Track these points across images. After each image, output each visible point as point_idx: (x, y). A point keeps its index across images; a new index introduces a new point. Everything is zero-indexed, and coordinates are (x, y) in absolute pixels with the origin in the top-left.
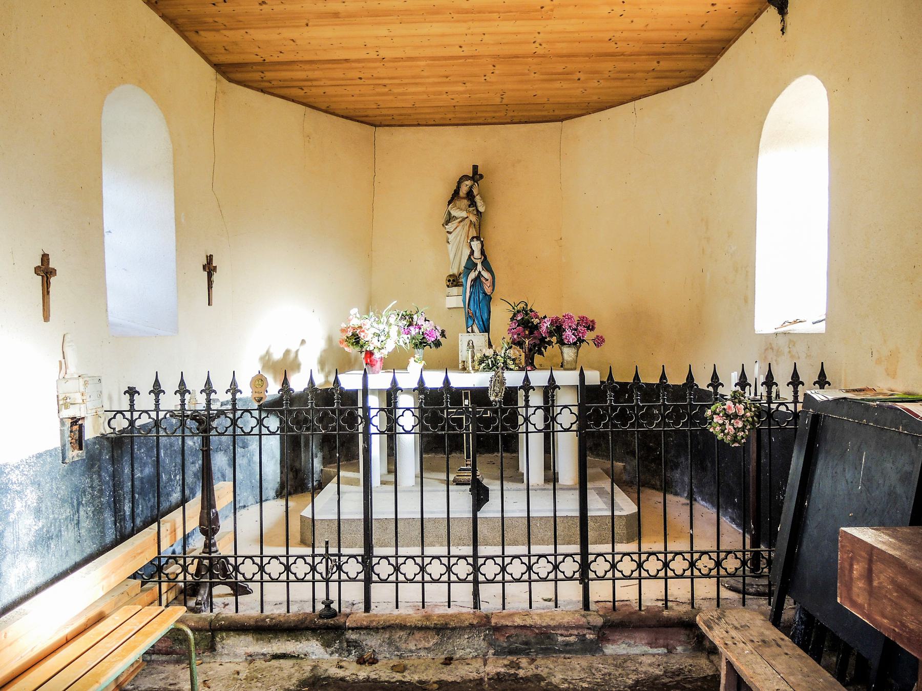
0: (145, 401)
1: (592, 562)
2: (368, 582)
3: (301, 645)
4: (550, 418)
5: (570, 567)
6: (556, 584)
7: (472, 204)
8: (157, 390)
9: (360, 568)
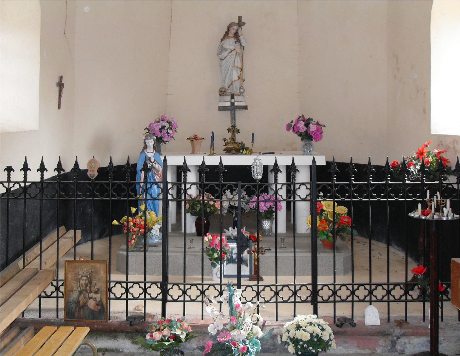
0: (17, 176)
1: (320, 290)
2: (164, 301)
3: (118, 343)
4: (291, 192)
5: (304, 294)
6: (335, 305)
7: (237, 41)
8: (26, 168)
9: (159, 291)
